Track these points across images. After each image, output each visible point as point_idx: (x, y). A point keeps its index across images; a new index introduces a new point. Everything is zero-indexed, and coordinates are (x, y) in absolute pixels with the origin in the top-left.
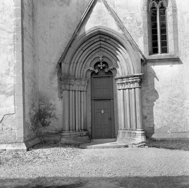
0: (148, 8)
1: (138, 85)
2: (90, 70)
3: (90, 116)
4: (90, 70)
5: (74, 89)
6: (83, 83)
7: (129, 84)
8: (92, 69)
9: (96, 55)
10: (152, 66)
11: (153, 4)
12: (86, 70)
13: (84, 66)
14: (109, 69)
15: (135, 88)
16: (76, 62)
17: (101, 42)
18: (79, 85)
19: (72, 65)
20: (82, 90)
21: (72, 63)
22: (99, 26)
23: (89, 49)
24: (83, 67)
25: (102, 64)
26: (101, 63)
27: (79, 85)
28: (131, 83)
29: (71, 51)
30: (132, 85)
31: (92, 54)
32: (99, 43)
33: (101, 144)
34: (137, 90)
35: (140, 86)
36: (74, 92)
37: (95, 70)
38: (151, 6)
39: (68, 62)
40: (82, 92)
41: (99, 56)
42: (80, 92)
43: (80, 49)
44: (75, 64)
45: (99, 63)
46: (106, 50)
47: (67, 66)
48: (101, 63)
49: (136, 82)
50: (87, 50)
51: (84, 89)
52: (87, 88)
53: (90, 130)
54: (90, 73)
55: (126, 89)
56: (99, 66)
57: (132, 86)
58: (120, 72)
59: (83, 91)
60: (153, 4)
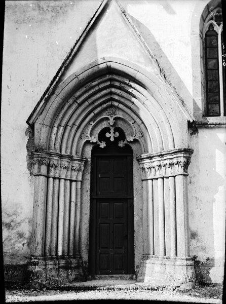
0: (201, 32)
1: (183, 171)
2: (91, 142)
3: (87, 191)
4: (91, 142)
5: (57, 176)
6: (76, 165)
7: (163, 168)
8: (94, 139)
9: (103, 115)
10: (218, 134)
11: (211, 26)
12: (83, 142)
13: (78, 134)
14: (126, 142)
15: (174, 177)
16: (64, 123)
17: (113, 90)
18: (66, 168)
19: (55, 129)
20: (74, 178)
21: (56, 125)
22: (110, 57)
23: (90, 101)
24: (78, 139)
25: (114, 133)
26: (112, 131)
27: (66, 168)
28: (157, 168)
29: (55, 101)
30: (169, 169)
31: (96, 111)
32: (108, 91)
33: (92, 199)
34: (179, 179)
35: (185, 171)
36: (57, 181)
37: (100, 143)
38: (206, 29)
39: (48, 121)
40: (74, 183)
41: (109, 117)
42: (69, 181)
43: (71, 101)
44: (62, 128)
45: (107, 130)
46: (121, 106)
47: (45, 130)
48: (112, 131)
49: (178, 163)
50: (87, 103)
51: (77, 178)
52: (83, 175)
53: (85, 256)
54: (89, 150)
55: (157, 179)
56: (108, 135)
57: (169, 172)
58: (154, 144)
59: (76, 181)
60: (211, 26)
